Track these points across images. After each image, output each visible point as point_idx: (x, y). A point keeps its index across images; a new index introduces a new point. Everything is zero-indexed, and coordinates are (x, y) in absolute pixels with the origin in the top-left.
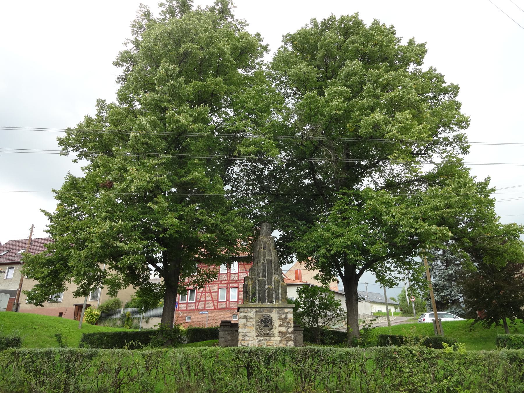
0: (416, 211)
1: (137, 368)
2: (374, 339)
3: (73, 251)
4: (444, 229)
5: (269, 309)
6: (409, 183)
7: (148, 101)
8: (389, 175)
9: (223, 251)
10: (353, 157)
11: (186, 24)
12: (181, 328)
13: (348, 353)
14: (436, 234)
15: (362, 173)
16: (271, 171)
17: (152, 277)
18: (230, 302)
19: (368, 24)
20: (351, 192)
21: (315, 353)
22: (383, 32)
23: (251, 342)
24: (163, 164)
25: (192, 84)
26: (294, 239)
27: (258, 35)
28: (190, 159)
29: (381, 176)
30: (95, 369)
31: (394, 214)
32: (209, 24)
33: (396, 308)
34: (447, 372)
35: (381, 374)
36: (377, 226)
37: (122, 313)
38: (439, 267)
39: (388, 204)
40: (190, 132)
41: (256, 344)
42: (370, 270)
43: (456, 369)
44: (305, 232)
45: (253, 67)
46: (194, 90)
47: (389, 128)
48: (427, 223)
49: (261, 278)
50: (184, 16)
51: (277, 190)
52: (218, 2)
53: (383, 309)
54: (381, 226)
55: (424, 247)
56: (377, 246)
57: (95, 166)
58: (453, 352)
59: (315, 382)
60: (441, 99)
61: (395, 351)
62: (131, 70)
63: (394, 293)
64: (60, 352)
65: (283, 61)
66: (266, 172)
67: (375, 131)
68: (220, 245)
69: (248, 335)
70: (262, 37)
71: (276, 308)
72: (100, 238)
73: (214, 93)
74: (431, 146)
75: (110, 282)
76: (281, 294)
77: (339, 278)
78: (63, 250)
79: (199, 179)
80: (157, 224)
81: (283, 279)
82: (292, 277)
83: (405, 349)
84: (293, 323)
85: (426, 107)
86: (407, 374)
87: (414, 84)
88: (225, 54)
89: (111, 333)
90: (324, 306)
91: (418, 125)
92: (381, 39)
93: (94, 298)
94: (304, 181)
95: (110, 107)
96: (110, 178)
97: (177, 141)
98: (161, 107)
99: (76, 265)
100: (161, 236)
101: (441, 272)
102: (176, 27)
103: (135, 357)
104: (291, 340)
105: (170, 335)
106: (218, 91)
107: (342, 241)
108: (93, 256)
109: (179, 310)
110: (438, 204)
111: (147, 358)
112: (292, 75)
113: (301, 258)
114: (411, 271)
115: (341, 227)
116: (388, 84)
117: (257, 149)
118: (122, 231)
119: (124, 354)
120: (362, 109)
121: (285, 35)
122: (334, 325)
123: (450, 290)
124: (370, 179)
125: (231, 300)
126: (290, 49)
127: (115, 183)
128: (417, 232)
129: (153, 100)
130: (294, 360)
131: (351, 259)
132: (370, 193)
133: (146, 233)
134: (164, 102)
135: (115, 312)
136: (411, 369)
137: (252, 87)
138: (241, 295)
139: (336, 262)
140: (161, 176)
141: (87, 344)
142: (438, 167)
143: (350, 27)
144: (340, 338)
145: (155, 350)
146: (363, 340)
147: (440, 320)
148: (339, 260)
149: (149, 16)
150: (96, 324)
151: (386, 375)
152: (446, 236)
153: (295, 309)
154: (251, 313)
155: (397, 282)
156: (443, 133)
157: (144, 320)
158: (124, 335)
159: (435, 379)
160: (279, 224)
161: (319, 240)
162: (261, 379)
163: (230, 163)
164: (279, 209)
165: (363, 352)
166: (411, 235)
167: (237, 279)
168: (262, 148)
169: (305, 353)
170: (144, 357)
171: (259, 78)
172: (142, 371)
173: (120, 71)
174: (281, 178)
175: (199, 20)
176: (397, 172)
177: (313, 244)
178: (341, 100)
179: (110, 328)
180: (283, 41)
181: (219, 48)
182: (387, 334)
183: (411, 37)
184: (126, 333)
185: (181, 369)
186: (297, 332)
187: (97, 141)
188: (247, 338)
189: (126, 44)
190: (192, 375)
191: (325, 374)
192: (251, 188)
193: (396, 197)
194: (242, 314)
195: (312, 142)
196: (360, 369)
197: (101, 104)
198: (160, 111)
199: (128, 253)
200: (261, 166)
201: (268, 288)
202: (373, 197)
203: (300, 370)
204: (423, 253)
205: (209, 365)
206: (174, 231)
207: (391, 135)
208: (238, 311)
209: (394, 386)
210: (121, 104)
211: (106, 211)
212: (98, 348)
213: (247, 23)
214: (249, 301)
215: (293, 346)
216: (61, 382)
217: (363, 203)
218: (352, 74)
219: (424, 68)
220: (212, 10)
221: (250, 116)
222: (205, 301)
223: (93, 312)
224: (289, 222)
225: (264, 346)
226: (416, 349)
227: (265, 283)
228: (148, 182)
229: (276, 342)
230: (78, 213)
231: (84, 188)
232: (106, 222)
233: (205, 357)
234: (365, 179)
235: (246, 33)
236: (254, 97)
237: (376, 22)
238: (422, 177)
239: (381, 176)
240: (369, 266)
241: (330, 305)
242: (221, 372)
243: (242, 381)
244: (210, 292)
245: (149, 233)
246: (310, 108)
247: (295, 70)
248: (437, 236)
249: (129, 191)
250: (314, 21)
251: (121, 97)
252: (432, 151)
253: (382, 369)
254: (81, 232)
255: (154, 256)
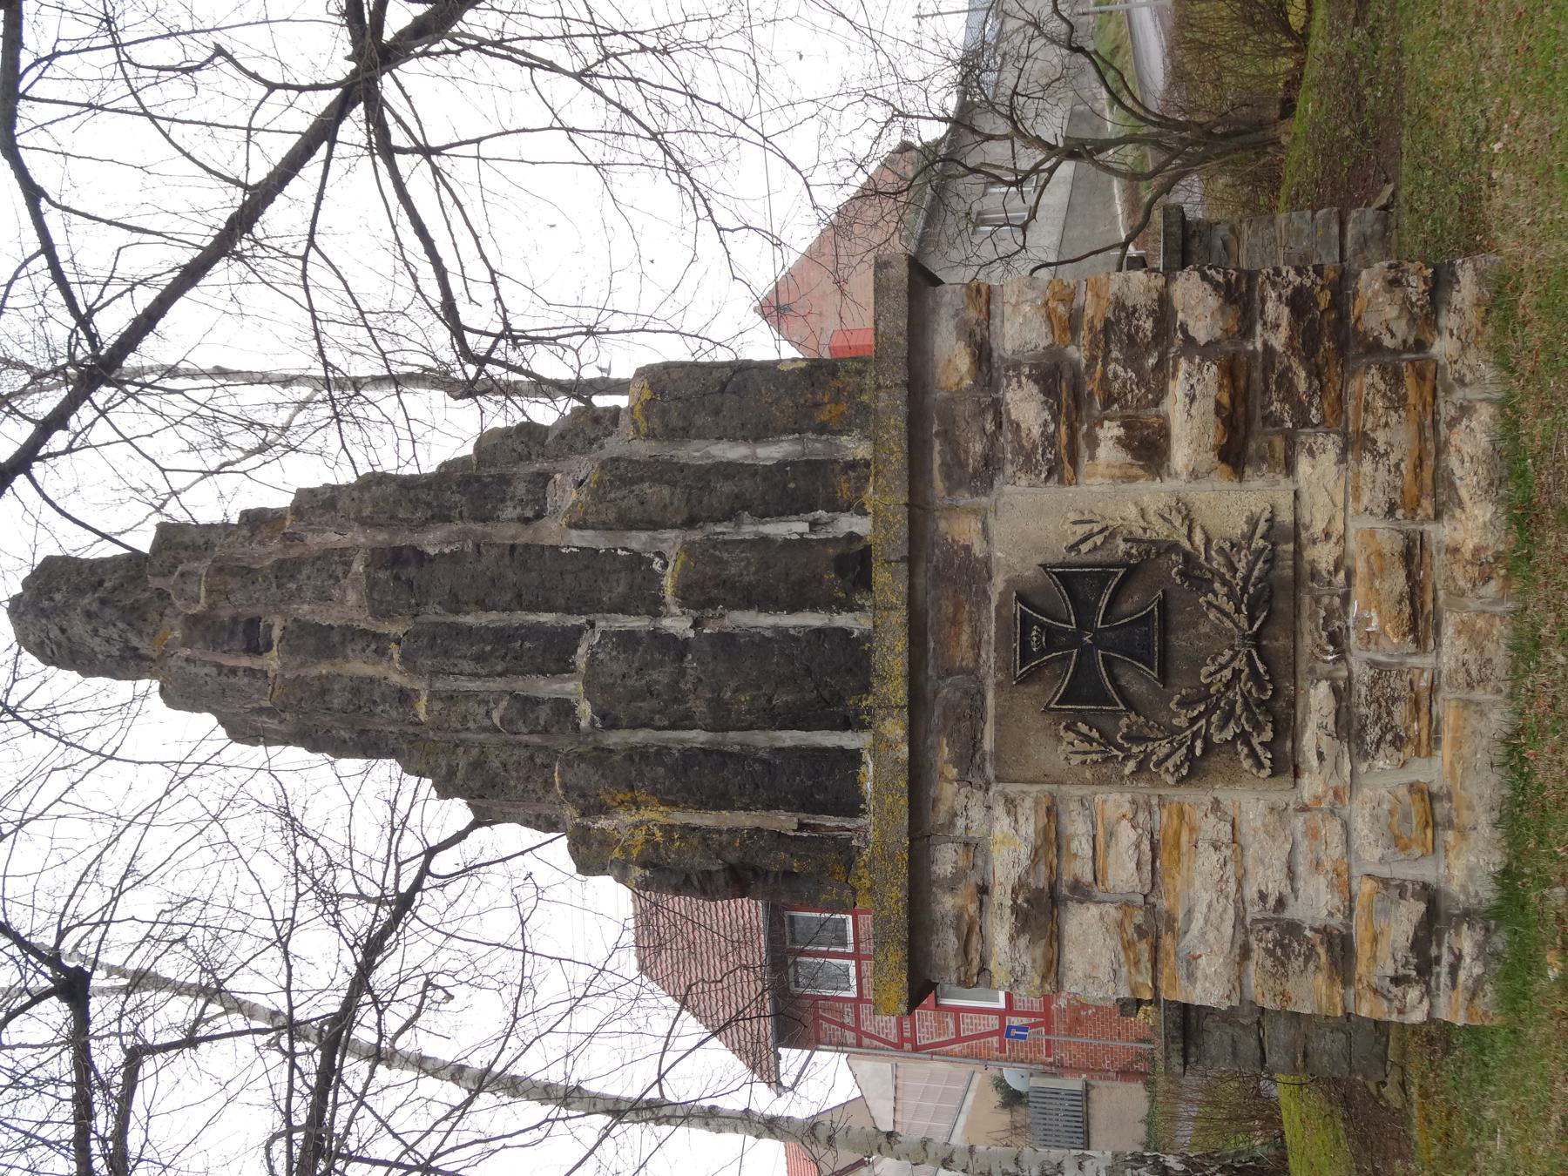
23: (1371, 853)
49: (571, 687)
69: (1275, 884)
188: (1315, 903)
227: (628, 639)
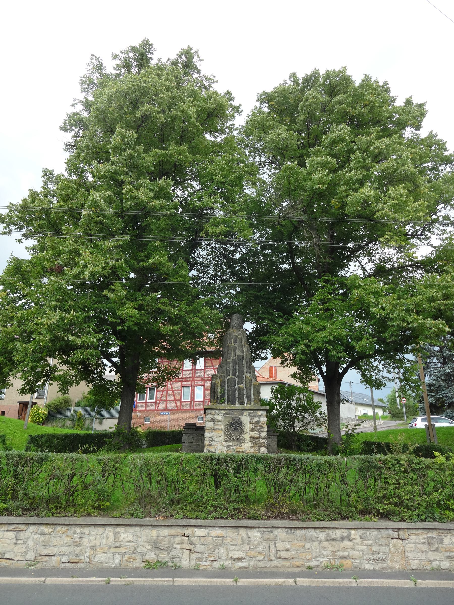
0: (408, 302)
1: (93, 475)
2: (357, 446)
3: (19, 344)
4: (441, 323)
5: (239, 412)
6: (402, 268)
7: (102, 173)
8: (379, 260)
9: (186, 345)
10: (339, 240)
11: (145, 82)
12: (140, 430)
13: (327, 462)
14: (431, 329)
15: (349, 256)
16: (243, 254)
17: (107, 372)
18: (194, 402)
19: (357, 80)
20: (334, 279)
21: (290, 461)
22: (375, 90)
23: (218, 448)
24: (120, 246)
25: (152, 153)
26: (269, 332)
27: (228, 93)
28: (150, 242)
29: (370, 261)
30: (46, 475)
31: (384, 305)
32: (171, 81)
33: (384, 411)
34: (437, 484)
35: (363, 486)
36: (364, 318)
37: (72, 412)
38: (435, 365)
39: (377, 294)
40: (150, 210)
41: (225, 450)
42: (355, 368)
43: (448, 481)
44: (282, 325)
45: (223, 133)
46: (155, 160)
47: (380, 205)
48: (421, 316)
49: (231, 376)
50: (143, 71)
51: (250, 276)
52: (182, 54)
53: (369, 412)
54: (369, 318)
55: (417, 343)
56: (363, 342)
57: (43, 248)
58: (445, 462)
59: (289, 493)
60: (442, 170)
61: (380, 461)
62: (81, 135)
63: (382, 394)
64: (7, 456)
65: (257, 125)
66: (238, 256)
67: (363, 208)
68: (185, 339)
70: (233, 95)
71: (247, 410)
72: (50, 330)
73: (178, 163)
74: (428, 226)
75: (60, 378)
76: (254, 395)
77: (320, 377)
78: (7, 343)
79: (161, 264)
80: (114, 315)
81: (255, 377)
82: (266, 374)
83: (392, 458)
84: (266, 427)
85: (424, 181)
86: (392, 486)
87: (411, 153)
88: (190, 117)
89: (61, 435)
90: (302, 409)
91: (414, 202)
92: (373, 99)
93: (41, 395)
94: (281, 266)
95: (59, 179)
96: (59, 262)
97: (135, 220)
98: (117, 181)
99: (22, 359)
100: (119, 328)
101: (436, 371)
102: (133, 85)
103: (90, 462)
104: (264, 446)
105: (127, 438)
106: (182, 161)
107: (323, 336)
108: (42, 350)
109: (136, 410)
110: (434, 295)
111: (104, 464)
112: (269, 141)
113: (276, 354)
114: (402, 371)
115: (324, 319)
116: (380, 153)
117: (228, 229)
118: (75, 323)
119: (78, 458)
120: (349, 183)
121: (260, 93)
122: (313, 429)
123: (446, 391)
124: (357, 264)
125: (195, 400)
126: (266, 110)
127: (65, 268)
128: (410, 326)
129: (108, 172)
130: (267, 469)
131: (333, 356)
132: (357, 281)
133: (101, 324)
134: (120, 175)
135: (64, 411)
136: (397, 480)
137: (221, 156)
138: (208, 394)
139: (316, 359)
140: (117, 261)
141: (34, 446)
142: (437, 250)
143: (337, 84)
144: (318, 445)
145: (112, 455)
146: (346, 447)
147: (434, 425)
148: (320, 357)
149: (101, 69)
150: (43, 424)
151: (370, 486)
152: (442, 331)
153: (268, 412)
154: (219, 416)
155: (386, 382)
156: (443, 211)
157: (97, 421)
158: (76, 437)
159: (424, 492)
160: (252, 316)
161: (298, 334)
162: (229, 489)
163: (195, 245)
164: (252, 298)
165: (345, 460)
166: (403, 330)
167: (203, 376)
168: (233, 228)
169: (279, 461)
170: (100, 463)
171: (229, 145)
172: (99, 478)
173: (68, 137)
174: (254, 262)
175: (159, 76)
176: (389, 256)
177: (291, 339)
178: (325, 172)
179: (58, 429)
180: (257, 101)
181: (183, 111)
182: (372, 440)
183: (408, 96)
184: (78, 435)
185: (141, 476)
186: (270, 437)
187: (43, 219)
188: (214, 443)
189: (74, 105)
190: (154, 483)
191: (301, 484)
192: (219, 274)
193: (386, 286)
194: (209, 417)
195: (291, 221)
196: (341, 479)
197: (48, 174)
198: (116, 185)
199: (80, 347)
200: (232, 248)
201: (239, 387)
202: (360, 286)
203: (274, 479)
204: (417, 350)
205: (172, 473)
206: (133, 323)
207: (382, 214)
208: (205, 413)
209: (378, 499)
210: (71, 176)
211: (56, 300)
212: (49, 451)
213: (215, 79)
214: (217, 402)
215: (266, 452)
216: (8, 488)
217: (348, 292)
218: (339, 141)
219: (423, 133)
220: (175, 63)
221: (219, 191)
222: (166, 400)
223: (40, 411)
224: (263, 313)
225: (234, 453)
226: (404, 458)
228: (104, 268)
229: (247, 448)
230: (24, 301)
231: (29, 272)
232: (56, 312)
233: (168, 463)
234: (352, 263)
235: (214, 92)
236: (224, 168)
237: (367, 78)
238: (418, 262)
239: (370, 261)
240: (354, 364)
241: (310, 407)
242: (186, 481)
243: (209, 490)
244: (172, 390)
245: (104, 324)
246: (289, 182)
247: (272, 136)
248: (432, 331)
249: (82, 277)
250: (294, 76)
251: (70, 168)
252: (430, 232)
253: (365, 480)
254: (27, 323)
255: (110, 350)
